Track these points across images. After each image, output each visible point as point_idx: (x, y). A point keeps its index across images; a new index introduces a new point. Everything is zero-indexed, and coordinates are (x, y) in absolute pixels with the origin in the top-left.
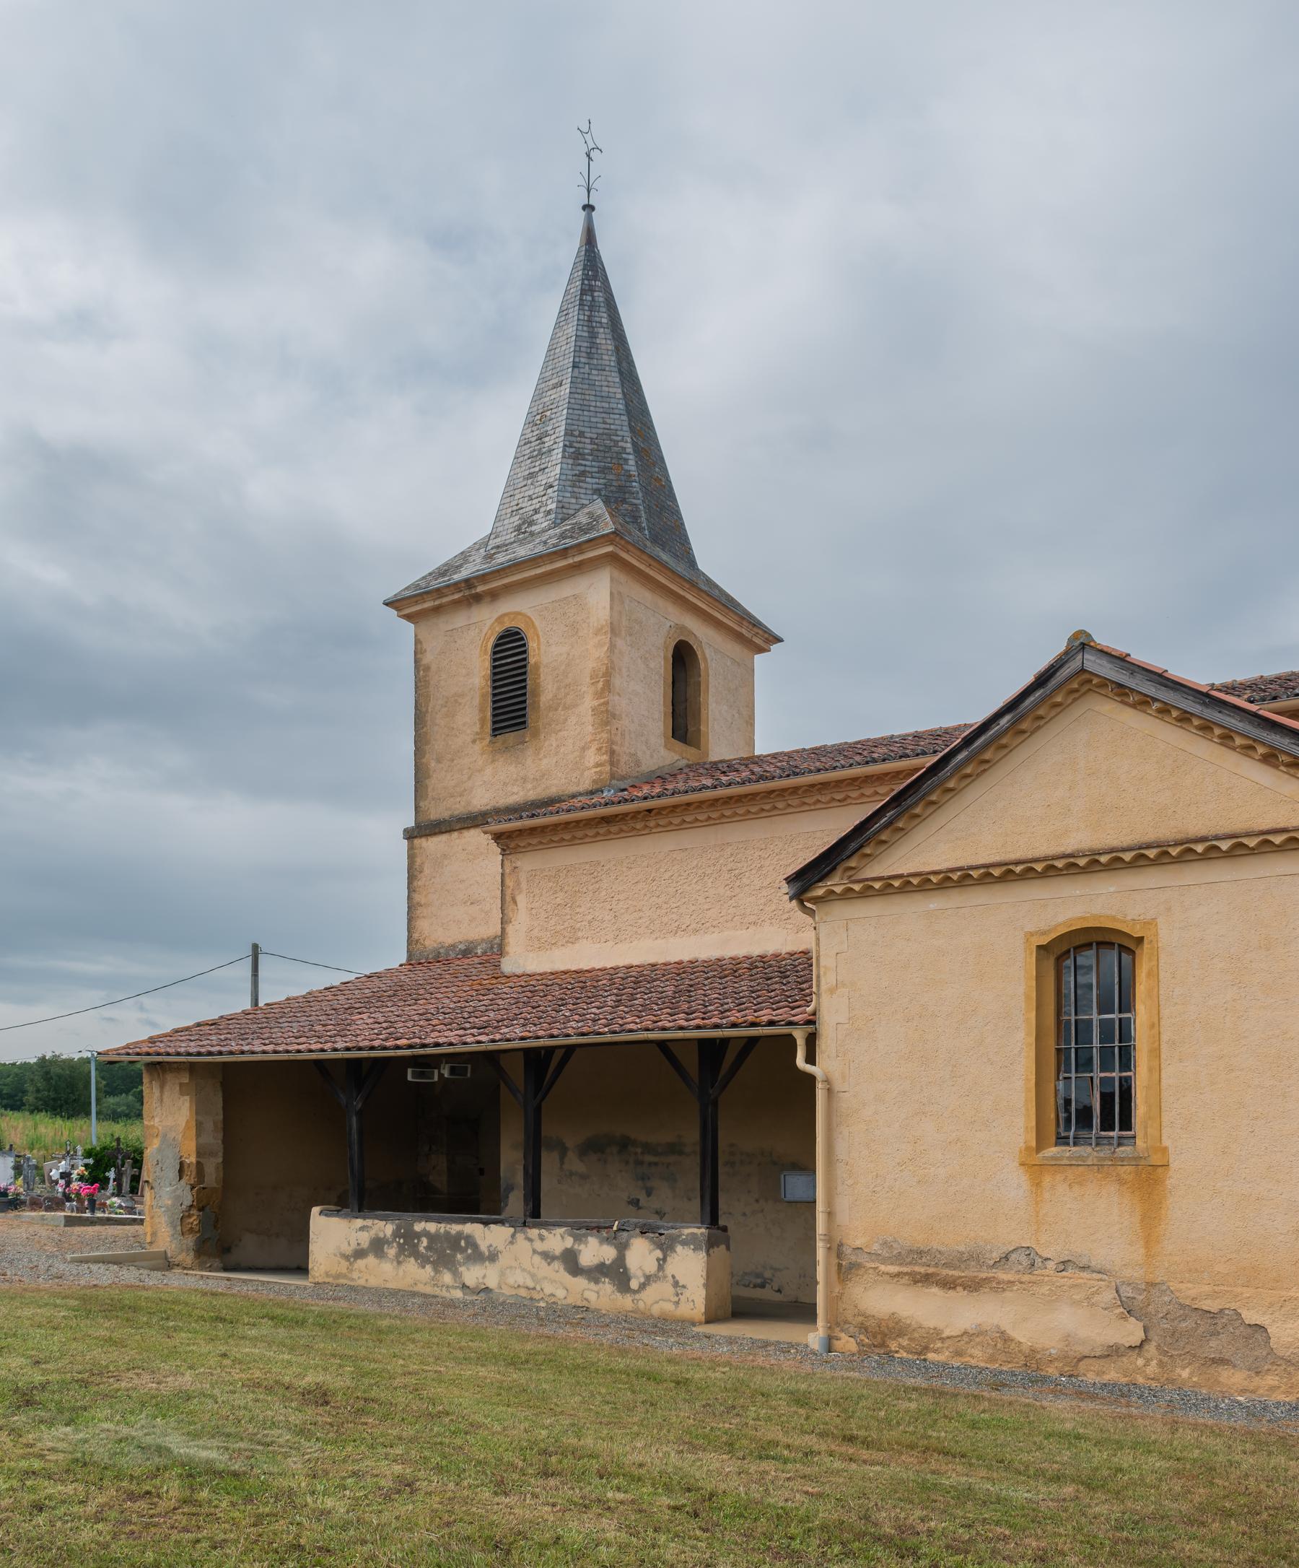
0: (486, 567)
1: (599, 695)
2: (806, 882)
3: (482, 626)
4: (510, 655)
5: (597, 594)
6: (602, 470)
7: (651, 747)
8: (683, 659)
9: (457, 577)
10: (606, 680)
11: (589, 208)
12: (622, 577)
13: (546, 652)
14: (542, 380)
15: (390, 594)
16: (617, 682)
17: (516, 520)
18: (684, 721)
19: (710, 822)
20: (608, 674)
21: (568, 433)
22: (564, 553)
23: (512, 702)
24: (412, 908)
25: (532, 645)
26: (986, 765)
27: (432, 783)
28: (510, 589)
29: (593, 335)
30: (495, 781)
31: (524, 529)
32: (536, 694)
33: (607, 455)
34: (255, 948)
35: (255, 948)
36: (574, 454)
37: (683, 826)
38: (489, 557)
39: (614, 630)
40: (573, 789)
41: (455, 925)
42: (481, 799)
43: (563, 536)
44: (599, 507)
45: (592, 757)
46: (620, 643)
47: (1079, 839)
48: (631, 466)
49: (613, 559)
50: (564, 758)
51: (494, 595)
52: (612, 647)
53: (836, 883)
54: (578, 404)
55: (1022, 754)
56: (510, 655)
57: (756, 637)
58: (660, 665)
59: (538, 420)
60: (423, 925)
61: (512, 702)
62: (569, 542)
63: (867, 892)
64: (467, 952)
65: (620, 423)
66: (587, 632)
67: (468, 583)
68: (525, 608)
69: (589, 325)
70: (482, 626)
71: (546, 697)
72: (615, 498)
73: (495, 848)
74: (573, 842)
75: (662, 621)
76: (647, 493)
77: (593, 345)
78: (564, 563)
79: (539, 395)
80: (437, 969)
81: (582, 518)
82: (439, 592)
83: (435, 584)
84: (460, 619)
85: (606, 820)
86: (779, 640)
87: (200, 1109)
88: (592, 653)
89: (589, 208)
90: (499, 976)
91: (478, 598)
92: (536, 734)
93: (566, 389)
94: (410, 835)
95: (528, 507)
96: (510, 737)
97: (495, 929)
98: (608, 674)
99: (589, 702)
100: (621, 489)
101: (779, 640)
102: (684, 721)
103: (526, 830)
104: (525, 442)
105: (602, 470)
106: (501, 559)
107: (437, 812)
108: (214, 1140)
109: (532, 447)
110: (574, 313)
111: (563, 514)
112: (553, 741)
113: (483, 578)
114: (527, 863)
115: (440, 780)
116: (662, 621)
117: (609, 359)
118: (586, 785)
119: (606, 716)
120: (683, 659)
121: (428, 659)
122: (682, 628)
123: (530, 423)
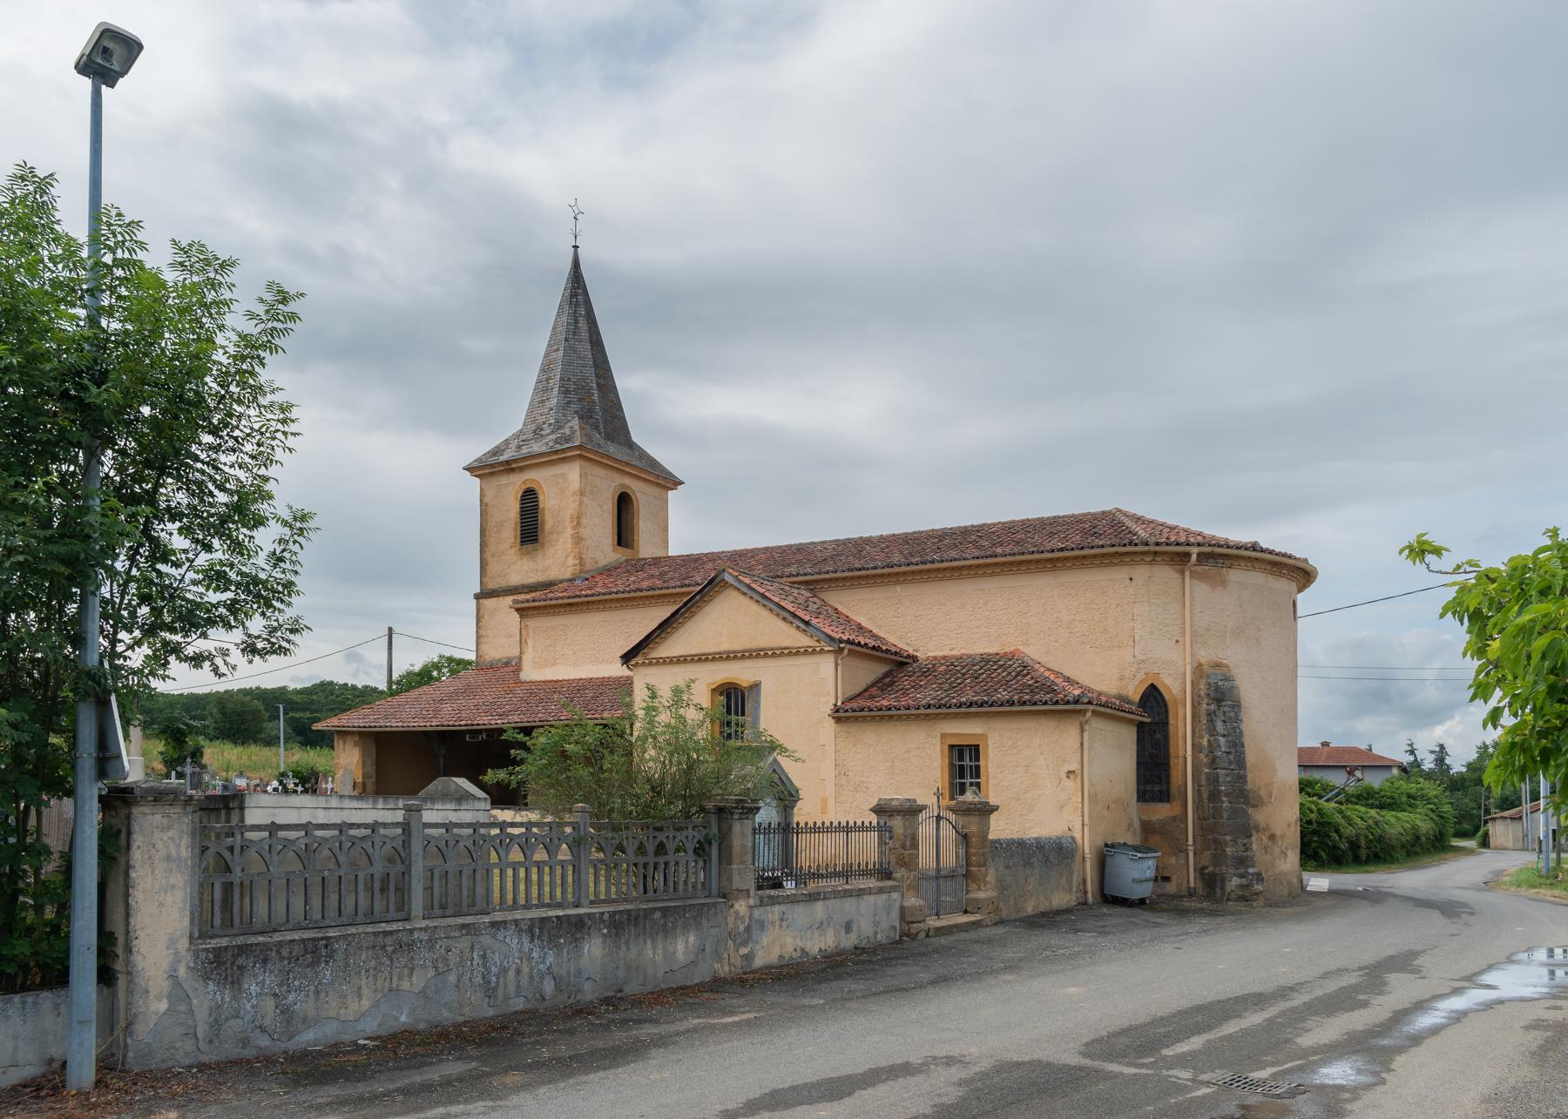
0: (517, 455)
1: (574, 528)
2: (627, 658)
3: (513, 486)
4: (530, 500)
5: (573, 473)
6: (580, 400)
7: (603, 550)
8: (624, 503)
9: (502, 458)
10: (578, 521)
11: (576, 247)
12: (584, 464)
13: (549, 502)
14: (549, 345)
15: (466, 463)
16: (584, 521)
17: (533, 427)
18: (624, 535)
19: (616, 609)
20: (579, 517)
21: (562, 379)
22: (556, 452)
23: (530, 530)
24: (478, 638)
25: (541, 498)
26: (693, 614)
27: (489, 568)
28: (529, 467)
29: (576, 322)
30: (522, 570)
31: (538, 432)
32: (543, 525)
33: (582, 390)
34: (390, 629)
35: (390, 629)
36: (565, 392)
37: (604, 610)
38: (519, 447)
39: (582, 493)
40: (562, 577)
41: (501, 648)
42: (515, 579)
43: (556, 442)
44: (575, 423)
45: (571, 561)
46: (585, 500)
47: (725, 646)
48: (596, 397)
49: (580, 456)
50: (556, 561)
51: (521, 469)
52: (581, 503)
53: (639, 659)
54: (567, 363)
55: (707, 609)
56: (530, 500)
57: (668, 481)
58: (610, 508)
59: (546, 369)
60: (484, 647)
61: (530, 530)
62: (559, 447)
63: (651, 664)
64: (507, 664)
65: (590, 372)
66: (569, 492)
67: (508, 462)
68: (539, 478)
69: (575, 316)
70: (513, 486)
71: (548, 527)
72: (586, 416)
73: (516, 616)
74: (554, 614)
75: (608, 485)
76: (604, 411)
77: (576, 327)
78: (555, 457)
79: (547, 355)
80: (490, 673)
81: (567, 431)
82: (492, 466)
83: (492, 460)
84: (504, 480)
85: (569, 605)
86: (681, 483)
87: (364, 754)
88: (571, 506)
89: (576, 247)
90: (519, 682)
91: (513, 470)
92: (543, 546)
93: (561, 353)
94: (478, 597)
95: (541, 419)
96: (530, 546)
97: (516, 652)
98: (579, 517)
99: (569, 532)
100: (590, 411)
101: (681, 483)
102: (624, 535)
103: (539, 602)
104: (539, 381)
105: (580, 400)
106: (525, 450)
107: (492, 585)
108: (371, 770)
109: (542, 386)
110: (566, 307)
111: (558, 426)
112: (551, 551)
113: (515, 461)
114: (533, 623)
115: (494, 567)
116: (608, 485)
117: (585, 335)
118: (568, 576)
119: (578, 540)
120: (624, 503)
121: (487, 500)
122: (623, 485)
123: (543, 370)
